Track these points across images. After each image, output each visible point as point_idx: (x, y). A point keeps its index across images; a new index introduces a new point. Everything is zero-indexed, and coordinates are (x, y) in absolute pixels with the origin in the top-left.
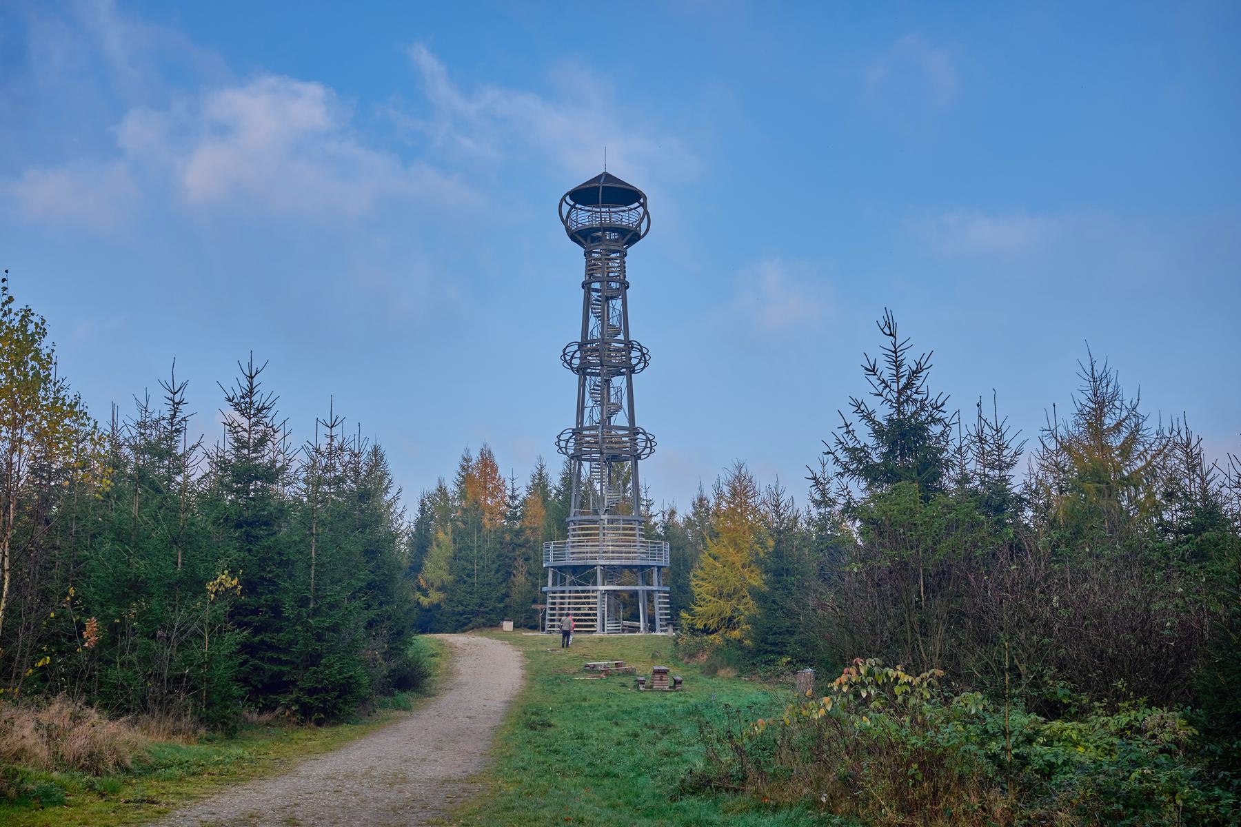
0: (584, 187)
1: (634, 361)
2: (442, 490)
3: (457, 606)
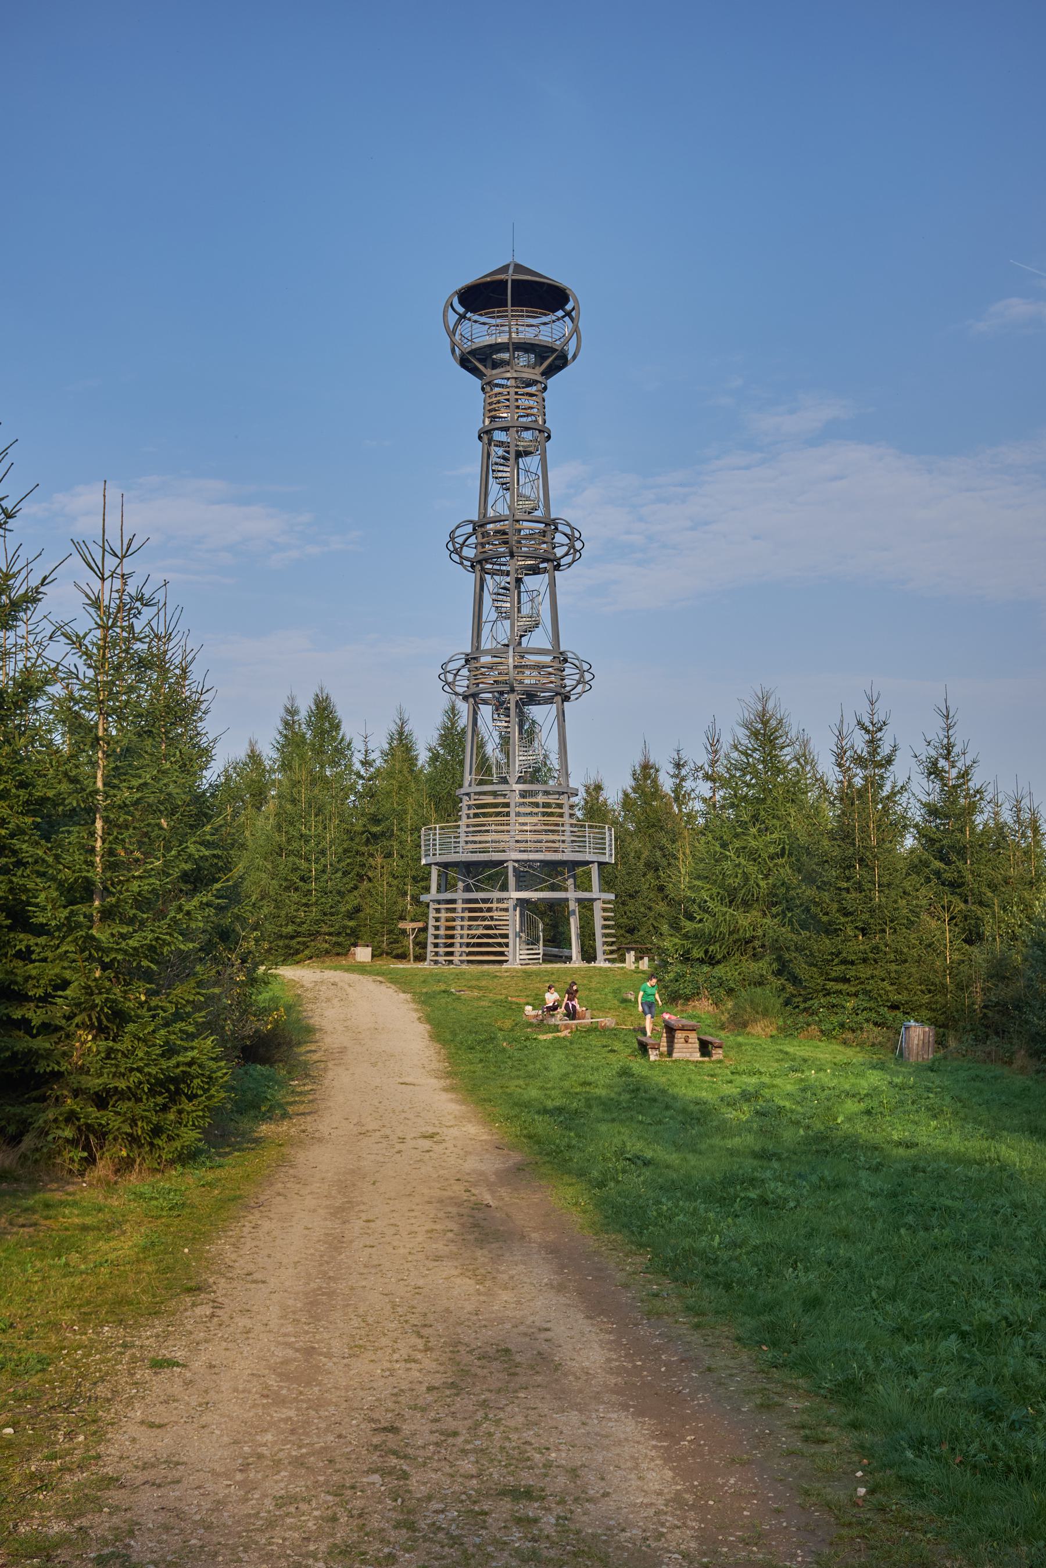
0: (489, 279)
1: (559, 552)
2: (254, 758)
3: (287, 925)
